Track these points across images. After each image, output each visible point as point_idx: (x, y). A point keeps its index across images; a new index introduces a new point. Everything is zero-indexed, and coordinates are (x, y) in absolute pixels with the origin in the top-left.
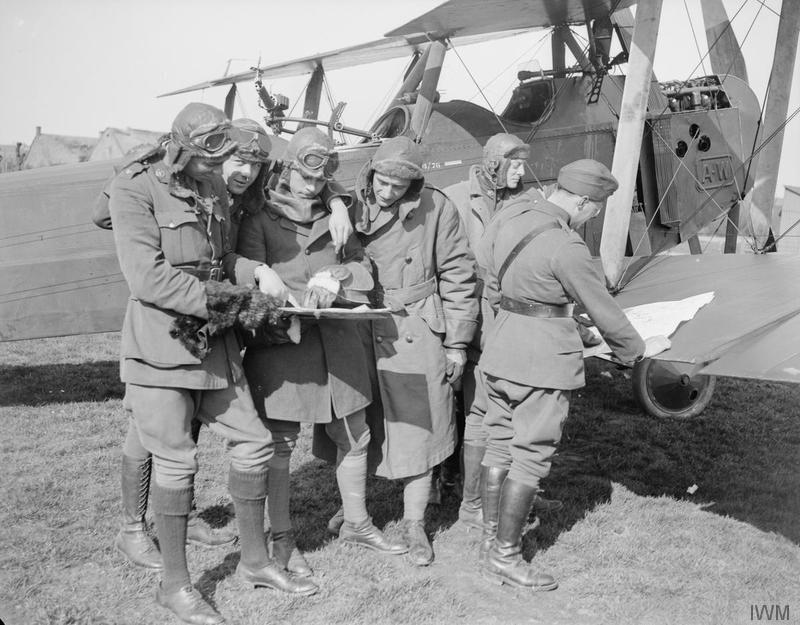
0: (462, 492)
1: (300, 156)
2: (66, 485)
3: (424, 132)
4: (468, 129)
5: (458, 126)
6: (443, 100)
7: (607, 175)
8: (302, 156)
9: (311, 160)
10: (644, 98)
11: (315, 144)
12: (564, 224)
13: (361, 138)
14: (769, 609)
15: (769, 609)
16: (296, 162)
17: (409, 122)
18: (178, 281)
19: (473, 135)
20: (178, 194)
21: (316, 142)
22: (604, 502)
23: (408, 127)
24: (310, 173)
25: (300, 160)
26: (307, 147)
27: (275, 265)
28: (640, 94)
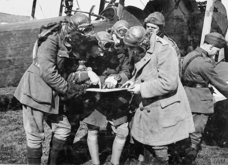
0: (96, 126)
1: (118, 29)
2: (9, 145)
3: (121, 17)
4: (136, 17)
5: (132, 15)
6: (142, 7)
7: (223, 38)
8: (118, 30)
9: (121, 32)
10: (213, 8)
11: (124, 26)
12: (204, 55)
13: (96, 18)
14: (219, 161)
15: (219, 161)
16: (115, 31)
17: (116, 13)
18: (59, 80)
19: (138, 18)
20: (66, 45)
21: (125, 26)
22: (205, 143)
23: (116, 15)
24: (120, 36)
25: (117, 31)
26: (121, 27)
27: (185, 86)
28: (211, 7)
